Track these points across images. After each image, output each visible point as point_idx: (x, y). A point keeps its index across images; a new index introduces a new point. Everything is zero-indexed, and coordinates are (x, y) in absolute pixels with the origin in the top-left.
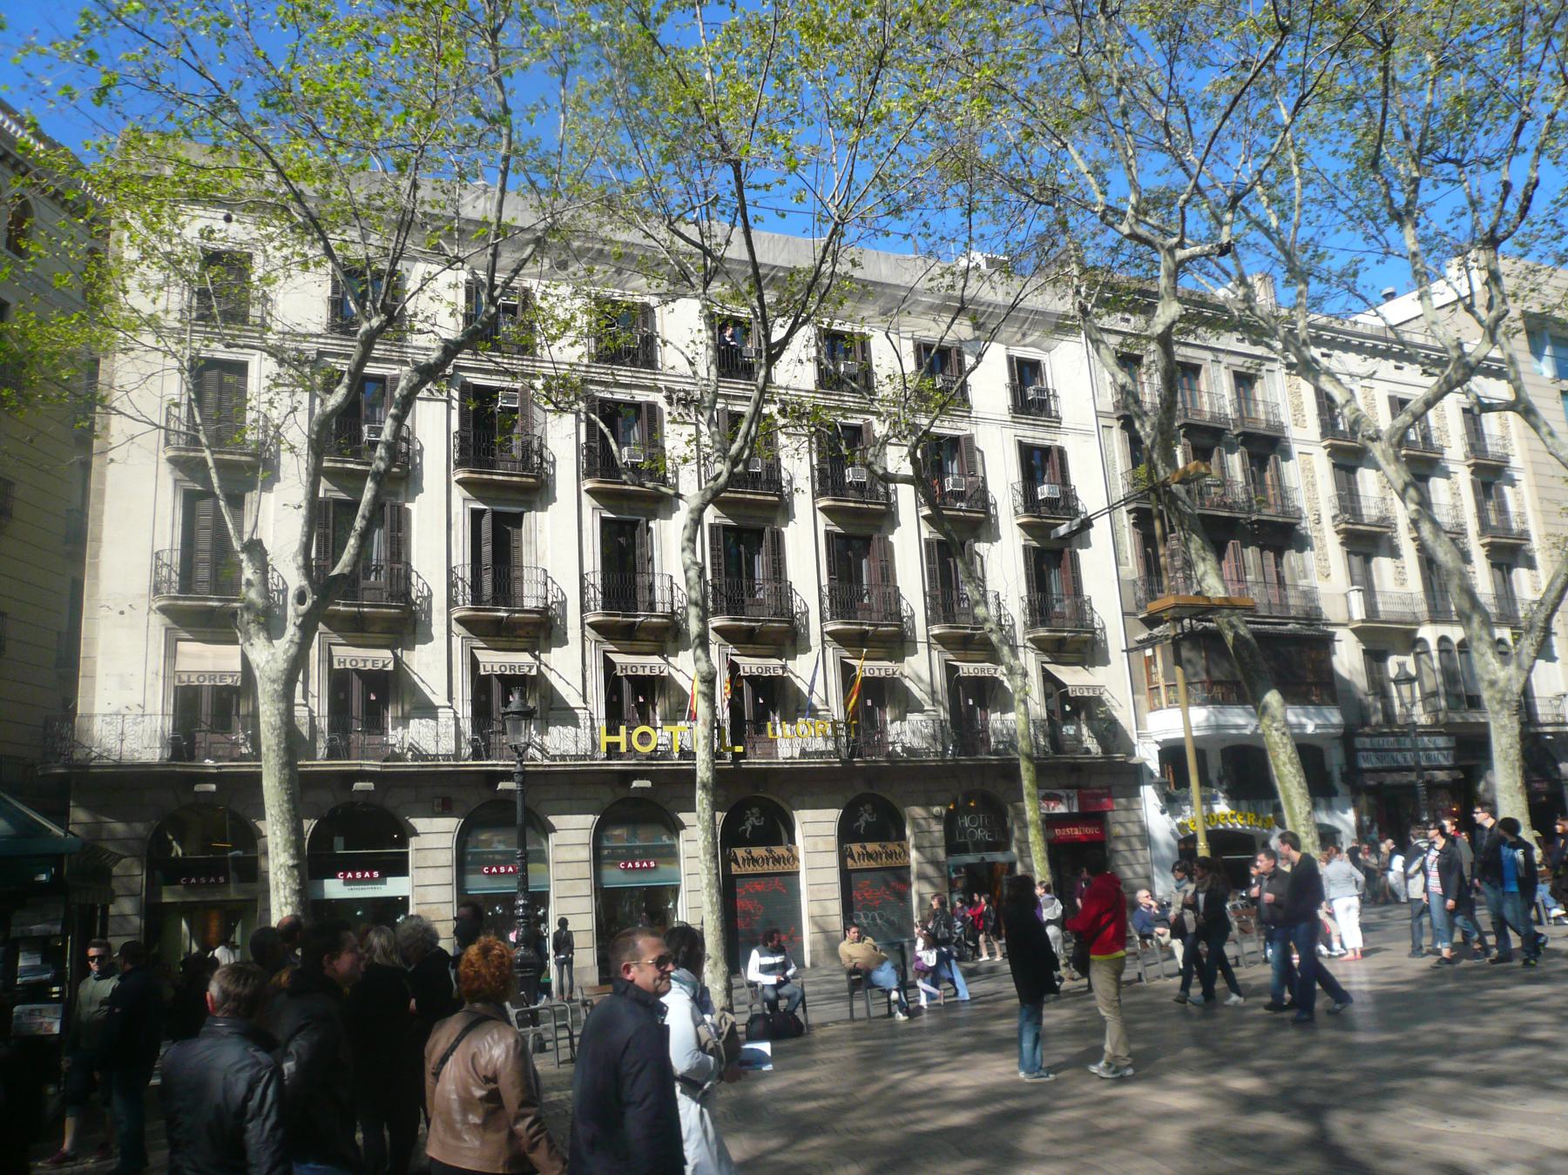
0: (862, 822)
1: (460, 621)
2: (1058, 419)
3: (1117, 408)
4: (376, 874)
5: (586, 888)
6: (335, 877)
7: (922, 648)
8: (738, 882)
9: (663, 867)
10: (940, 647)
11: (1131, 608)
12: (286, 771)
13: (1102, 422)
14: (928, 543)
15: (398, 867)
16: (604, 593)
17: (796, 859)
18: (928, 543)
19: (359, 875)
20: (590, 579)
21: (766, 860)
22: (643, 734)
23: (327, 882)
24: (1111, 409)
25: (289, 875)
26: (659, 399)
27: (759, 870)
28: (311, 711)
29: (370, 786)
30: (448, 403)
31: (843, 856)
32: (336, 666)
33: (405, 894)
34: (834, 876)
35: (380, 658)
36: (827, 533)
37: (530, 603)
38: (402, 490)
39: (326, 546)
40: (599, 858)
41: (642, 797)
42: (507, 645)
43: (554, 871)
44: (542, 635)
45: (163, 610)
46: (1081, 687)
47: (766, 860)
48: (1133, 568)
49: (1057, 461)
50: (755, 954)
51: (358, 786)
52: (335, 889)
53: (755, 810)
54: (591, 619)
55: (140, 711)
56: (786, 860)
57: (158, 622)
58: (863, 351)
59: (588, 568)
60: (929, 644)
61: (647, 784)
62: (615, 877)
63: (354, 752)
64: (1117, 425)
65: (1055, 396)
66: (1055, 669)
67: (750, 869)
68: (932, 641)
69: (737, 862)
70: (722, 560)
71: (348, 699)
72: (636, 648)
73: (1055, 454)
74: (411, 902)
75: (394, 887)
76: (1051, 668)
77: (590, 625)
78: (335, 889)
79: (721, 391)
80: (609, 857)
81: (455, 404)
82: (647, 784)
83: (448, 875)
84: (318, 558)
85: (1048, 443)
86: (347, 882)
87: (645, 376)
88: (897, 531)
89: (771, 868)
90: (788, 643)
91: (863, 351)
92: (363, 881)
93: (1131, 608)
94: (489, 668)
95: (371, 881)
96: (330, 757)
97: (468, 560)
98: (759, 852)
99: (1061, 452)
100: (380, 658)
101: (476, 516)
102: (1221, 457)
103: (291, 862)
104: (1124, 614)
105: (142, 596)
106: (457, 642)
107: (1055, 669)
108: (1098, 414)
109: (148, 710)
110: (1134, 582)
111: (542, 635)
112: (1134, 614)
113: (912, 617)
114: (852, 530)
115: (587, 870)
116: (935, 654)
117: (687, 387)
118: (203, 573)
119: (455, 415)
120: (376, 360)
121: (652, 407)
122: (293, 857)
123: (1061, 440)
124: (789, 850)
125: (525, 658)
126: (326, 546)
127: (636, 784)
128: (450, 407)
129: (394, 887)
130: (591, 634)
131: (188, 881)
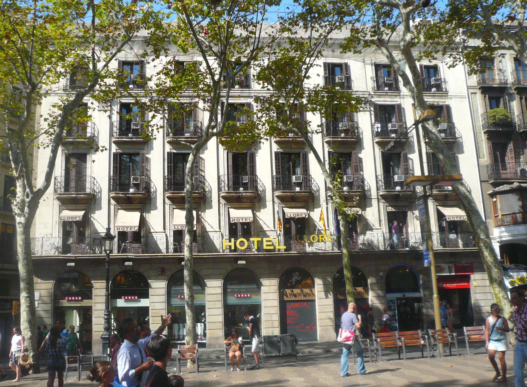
0: (294, 280)
1: (223, 197)
2: (447, 92)
3: (478, 84)
4: (136, 297)
5: (220, 305)
6: (121, 298)
7: (374, 202)
8: (288, 304)
9: (254, 297)
10: (383, 201)
11: (486, 178)
12: (25, 261)
13: (471, 91)
14: (169, 154)
15: (146, 295)
16: (385, 184)
17: (314, 295)
18: (276, 153)
19: (130, 298)
20: (222, 178)
21: (300, 295)
22: (242, 242)
23: (118, 300)
24: (476, 85)
25: (26, 300)
26: (251, 101)
27: (297, 299)
28: (166, 235)
29: (131, 263)
30: (370, 111)
31: (282, 295)
33: (148, 305)
34: (276, 303)
35: (301, 212)
36: (329, 152)
37: (88, 191)
38: (146, 147)
39: (116, 171)
40: (225, 293)
41: (242, 269)
43: (208, 298)
44: (202, 202)
45: (58, 199)
46: (453, 216)
47: (300, 295)
48: (486, 159)
49: (446, 112)
50: (464, 328)
51: (127, 263)
52: (121, 303)
53: (297, 273)
54: (222, 195)
55: (51, 236)
56: (309, 295)
57: (57, 203)
58: (346, 71)
59: (221, 173)
60: (378, 199)
61: (244, 262)
62: (232, 300)
63: (128, 251)
64: (479, 92)
65: (445, 82)
66: (441, 209)
67: (293, 298)
68: (380, 197)
69: (287, 296)
70: (280, 167)
71: (290, 228)
72: (242, 206)
73: (445, 109)
74: (150, 308)
75: (144, 303)
76: (439, 208)
77: (222, 197)
78: (121, 303)
79: (230, 94)
80: (231, 292)
81: (373, 113)
82: (244, 262)
83: (164, 298)
84: (113, 176)
85: (441, 104)
86: (126, 301)
87: (246, 92)
88: (363, 151)
89: (302, 298)
90: (311, 201)
91: (346, 71)
92: (131, 301)
93: (486, 178)
94: (289, 215)
95: (135, 301)
97: (63, 174)
98: (296, 291)
99: (448, 108)
100: (301, 212)
102: (505, 103)
103: (26, 295)
104: (481, 182)
105: (51, 194)
106: (167, 207)
107: (441, 209)
108: (469, 88)
109: (54, 236)
110: (487, 166)
111: (202, 202)
112: (487, 181)
114: (288, 151)
115: (220, 297)
116: (381, 205)
117: (264, 95)
118: (73, 184)
119: (373, 116)
120: (233, 97)
121: (249, 105)
122: (27, 293)
123: (448, 102)
124: (311, 291)
125: (304, 211)
126: (116, 171)
127: (239, 262)
128: (371, 114)
129: (144, 303)
130: (223, 201)
131: (68, 298)
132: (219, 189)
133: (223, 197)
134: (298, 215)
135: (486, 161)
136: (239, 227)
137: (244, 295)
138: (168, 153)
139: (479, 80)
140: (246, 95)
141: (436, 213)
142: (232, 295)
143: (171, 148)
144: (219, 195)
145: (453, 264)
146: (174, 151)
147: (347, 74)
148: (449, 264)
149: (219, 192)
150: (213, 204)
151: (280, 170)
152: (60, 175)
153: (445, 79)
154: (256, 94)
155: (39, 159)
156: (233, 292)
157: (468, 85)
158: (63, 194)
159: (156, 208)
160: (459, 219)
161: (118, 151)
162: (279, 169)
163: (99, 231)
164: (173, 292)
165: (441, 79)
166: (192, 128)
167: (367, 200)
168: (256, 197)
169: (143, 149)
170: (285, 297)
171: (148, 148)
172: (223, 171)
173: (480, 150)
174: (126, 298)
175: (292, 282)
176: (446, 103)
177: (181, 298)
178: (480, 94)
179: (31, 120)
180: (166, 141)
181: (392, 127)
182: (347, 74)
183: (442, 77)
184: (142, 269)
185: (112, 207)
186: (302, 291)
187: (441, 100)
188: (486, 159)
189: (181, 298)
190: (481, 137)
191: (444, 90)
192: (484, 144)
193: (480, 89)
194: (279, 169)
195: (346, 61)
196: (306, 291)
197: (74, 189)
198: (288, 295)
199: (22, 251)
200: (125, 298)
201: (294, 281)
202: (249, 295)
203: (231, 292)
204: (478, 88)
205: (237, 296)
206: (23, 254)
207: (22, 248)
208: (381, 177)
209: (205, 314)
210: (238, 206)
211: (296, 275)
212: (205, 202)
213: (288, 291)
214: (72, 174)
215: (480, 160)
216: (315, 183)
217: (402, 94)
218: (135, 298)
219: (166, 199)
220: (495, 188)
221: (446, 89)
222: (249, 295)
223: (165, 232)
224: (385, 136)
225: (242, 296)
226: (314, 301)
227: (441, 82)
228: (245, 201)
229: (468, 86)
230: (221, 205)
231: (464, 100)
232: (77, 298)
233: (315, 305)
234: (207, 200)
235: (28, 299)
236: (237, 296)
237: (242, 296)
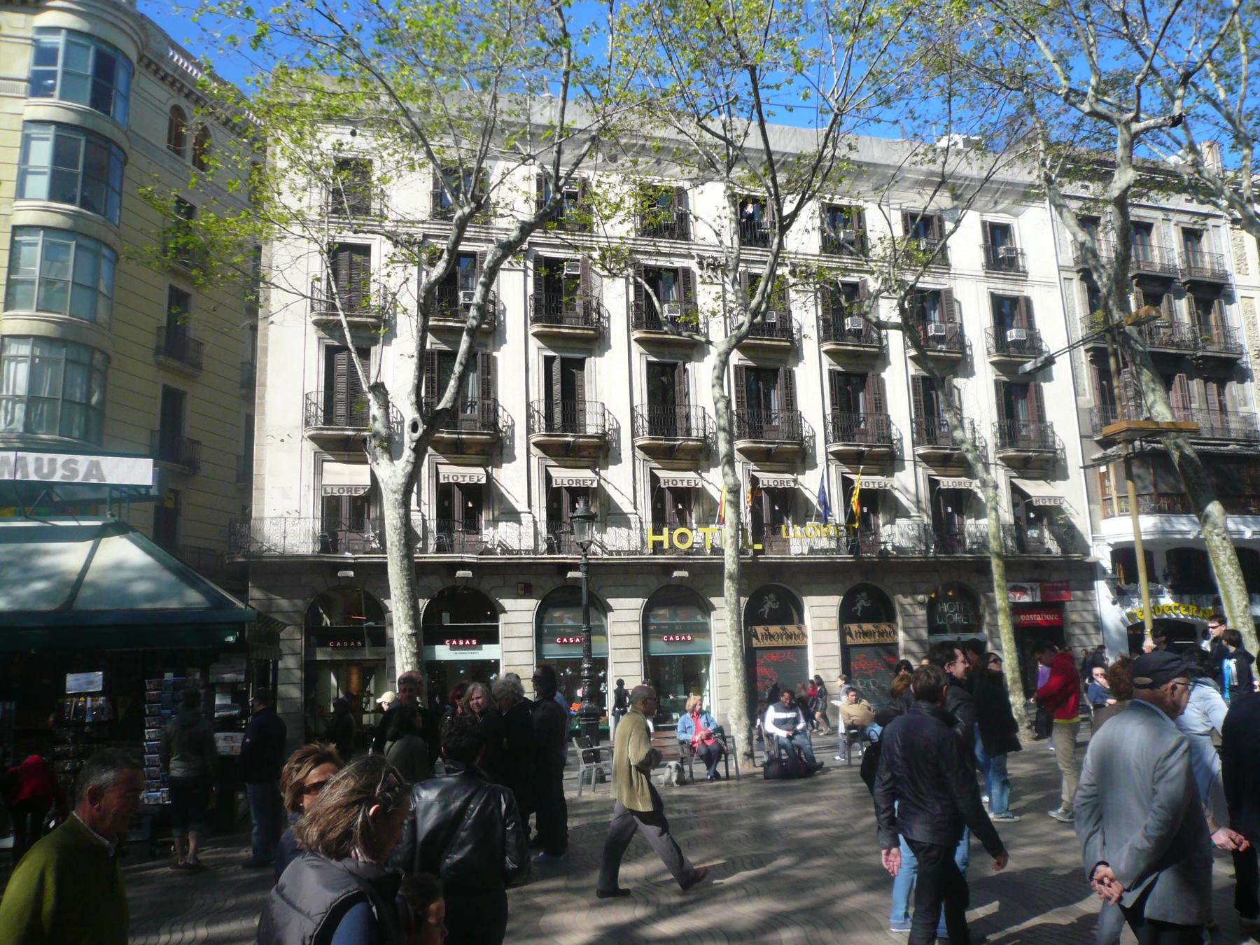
1: (537, 445)
2: (1025, 273)
3: (1076, 263)
4: (474, 642)
5: (637, 655)
6: (443, 643)
7: (909, 465)
9: (698, 640)
10: (924, 465)
12: (405, 562)
13: (1064, 274)
14: (914, 379)
15: (491, 636)
16: (650, 422)
17: (804, 635)
19: (461, 642)
20: (639, 410)
22: (682, 534)
24: (1072, 264)
25: (410, 642)
27: (774, 643)
28: (423, 516)
29: (469, 573)
32: (442, 481)
34: (836, 650)
35: (475, 474)
37: (591, 430)
39: (433, 388)
41: (681, 584)
42: (573, 463)
43: (612, 642)
44: (601, 456)
45: (312, 438)
46: (1043, 498)
48: (1090, 398)
49: (1024, 309)
51: (460, 573)
52: (443, 652)
53: (772, 596)
56: (796, 636)
57: (310, 447)
58: (859, 221)
59: (637, 402)
61: (685, 574)
62: (660, 647)
63: (456, 548)
64: (1076, 277)
65: (1022, 254)
67: (768, 643)
68: (918, 459)
73: (1022, 303)
75: (488, 652)
76: (1018, 482)
78: (443, 652)
80: (655, 631)
81: (530, 273)
82: (685, 574)
83: (530, 643)
84: (427, 397)
86: (453, 648)
87: (681, 246)
90: (798, 461)
91: (859, 221)
92: (464, 647)
93: (1088, 432)
95: (471, 647)
96: (711, 554)
97: (322, 388)
99: (1028, 301)
100: (475, 474)
101: (548, 361)
104: (1081, 437)
105: (296, 427)
106: (534, 461)
110: (1091, 410)
112: (1090, 437)
113: (900, 440)
115: (637, 642)
116: (920, 470)
118: (341, 409)
119: (530, 281)
120: (468, 240)
121: (687, 271)
123: (1027, 291)
124: (800, 629)
126: (433, 388)
127: (676, 574)
129: (488, 652)
130: (640, 454)
132: (530, 430)
133: (641, 447)
134: (578, 481)
135: (1089, 402)
136: (1116, 514)
137: (680, 637)
138: (736, 367)
139: (1078, 257)
140: (683, 251)
141: (1009, 487)
142: (657, 637)
143: (541, 345)
144: (633, 443)
145: (1038, 584)
146: (750, 363)
147: (860, 227)
148: (1032, 584)
149: (528, 433)
150: (623, 456)
151: (745, 400)
152: (315, 389)
153: (1022, 249)
154: (699, 252)
155: (269, 353)
156: (660, 632)
157: (1061, 264)
158: (321, 429)
159: (618, 460)
160: (1052, 504)
161: (741, 363)
162: (742, 398)
163: (625, 511)
164: (546, 631)
165: (1016, 249)
166: (579, 310)
167: (896, 462)
168: (494, 444)
169: (486, 346)
170: (754, 640)
171: (494, 340)
172: (537, 393)
173: (1079, 381)
174: (454, 642)
175: (764, 612)
176: (1025, 294)
177: (668, 640)
178: (1079, 282)
179: (1230, 337)
180: (530, 332)
181: (936, 331)
182: (860, 227)
183: (1018, 246)
184: (486, 586)
185: (534, 461)
186: (784, 629)
187: (1017, 288)
188: (1088, 396)
189: (668, 640)
190: (1080, 358)
191: (1021, 269)
192: (1085, 370)
193: (1078, 272)
194: (742, 398)
195: (860, 203)
196: (884, 627)
197: (343, 420)
198: (760, 637)
199: (400, 540)
200: (451, 643)
201: (767, 611)
202: (689, 638)
203: (655, 631)
204: (1075, 269)
205: (668, 638)
206: (402, 548)
207: (399, 534)
208: (643, 410)
209: (605, 676)
210: (460, 461)
211: (862, 598)
212: (606, 456)
213: (760, 630)
214: (339, 389)
215: (1079, 398)
216: (807, 425)
217: (952, 271)
218: (471, 642)
219: (532, 447)
220: (1105, 449)
221: (1024, 267)
222: (689, 638)
223: (530, 513)
224: (654, 328)
225: (677, 638)
226: (805, 647)
227: (1017, 254)
228: (681, 456)
229: (1059, 266)
230: (637, 462)
231: (1054, 289)
232: (683, 638)
233: (806, 655)
234: (611, 451)
235: (414, 640)
236: (668, 638)
237: (677, 638)
